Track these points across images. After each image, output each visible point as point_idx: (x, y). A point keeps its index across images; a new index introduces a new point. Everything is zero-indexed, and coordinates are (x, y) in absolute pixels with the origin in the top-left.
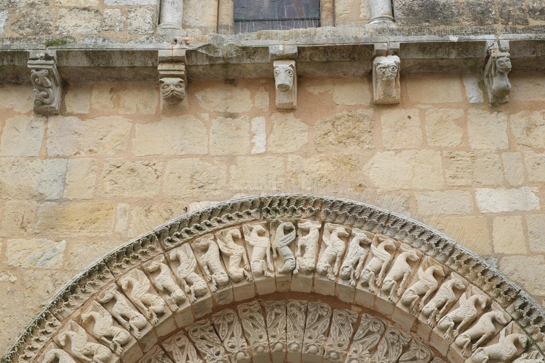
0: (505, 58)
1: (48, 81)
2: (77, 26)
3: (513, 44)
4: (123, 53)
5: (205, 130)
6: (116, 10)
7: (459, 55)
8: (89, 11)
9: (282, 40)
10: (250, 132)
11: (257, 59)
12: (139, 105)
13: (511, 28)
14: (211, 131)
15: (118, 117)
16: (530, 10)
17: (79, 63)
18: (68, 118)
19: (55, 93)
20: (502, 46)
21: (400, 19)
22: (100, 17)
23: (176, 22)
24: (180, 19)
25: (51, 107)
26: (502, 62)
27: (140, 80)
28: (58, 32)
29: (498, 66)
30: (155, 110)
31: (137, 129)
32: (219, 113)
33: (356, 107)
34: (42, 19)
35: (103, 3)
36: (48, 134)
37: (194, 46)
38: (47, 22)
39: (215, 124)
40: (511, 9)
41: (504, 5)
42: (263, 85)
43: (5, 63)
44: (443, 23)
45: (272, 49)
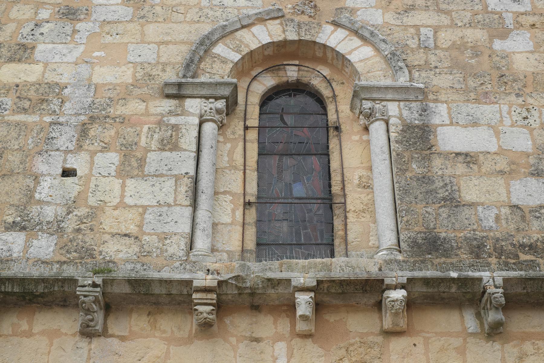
0: (499, 294)
1: (94, 306)
2: (118, 251)
3: (506, 281)
4: (162, 282)
5: (232, 354)
6: (153, 236)
7: (458, 289)
8: (129, 237)
9: (302, 272)
10: (273, 356)
11: (281, 290)
12: (173, 328)
13: (504, 261)
14: (238, 354)
15: (155, 339)
16: (521, 245)
17: (122, 290)
18: (110, 340)
19: (99, 316)
20: (496, 283)
21: (406, 251)
22: (139, 243)
23: (206, 248)
24: (209, 245)
25: (95, 330)
26: (497, 298)
27: (175, 304)
28: (101, 257)
29: (493, 301)
30: (187, 334)
31: (172, 351)
32: (245, 338)
33: (367, 334)
34: (88, 244)
35: (142, 230)
36: (92, 354)
37: (225, 276)
38: (92, 247)
39: (242, 347)
40: (503, 243)
41: (498, 240)
42: (284, 311)
43: (56, 288)
44: (443, 256)
45: (294, 281)
